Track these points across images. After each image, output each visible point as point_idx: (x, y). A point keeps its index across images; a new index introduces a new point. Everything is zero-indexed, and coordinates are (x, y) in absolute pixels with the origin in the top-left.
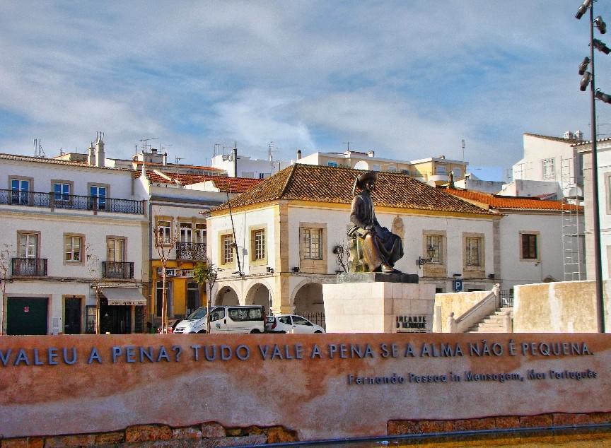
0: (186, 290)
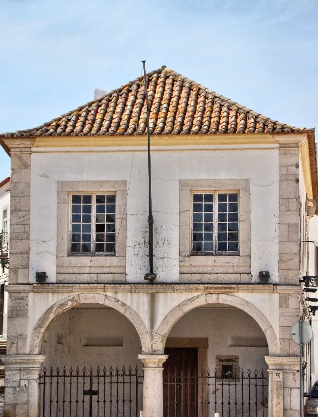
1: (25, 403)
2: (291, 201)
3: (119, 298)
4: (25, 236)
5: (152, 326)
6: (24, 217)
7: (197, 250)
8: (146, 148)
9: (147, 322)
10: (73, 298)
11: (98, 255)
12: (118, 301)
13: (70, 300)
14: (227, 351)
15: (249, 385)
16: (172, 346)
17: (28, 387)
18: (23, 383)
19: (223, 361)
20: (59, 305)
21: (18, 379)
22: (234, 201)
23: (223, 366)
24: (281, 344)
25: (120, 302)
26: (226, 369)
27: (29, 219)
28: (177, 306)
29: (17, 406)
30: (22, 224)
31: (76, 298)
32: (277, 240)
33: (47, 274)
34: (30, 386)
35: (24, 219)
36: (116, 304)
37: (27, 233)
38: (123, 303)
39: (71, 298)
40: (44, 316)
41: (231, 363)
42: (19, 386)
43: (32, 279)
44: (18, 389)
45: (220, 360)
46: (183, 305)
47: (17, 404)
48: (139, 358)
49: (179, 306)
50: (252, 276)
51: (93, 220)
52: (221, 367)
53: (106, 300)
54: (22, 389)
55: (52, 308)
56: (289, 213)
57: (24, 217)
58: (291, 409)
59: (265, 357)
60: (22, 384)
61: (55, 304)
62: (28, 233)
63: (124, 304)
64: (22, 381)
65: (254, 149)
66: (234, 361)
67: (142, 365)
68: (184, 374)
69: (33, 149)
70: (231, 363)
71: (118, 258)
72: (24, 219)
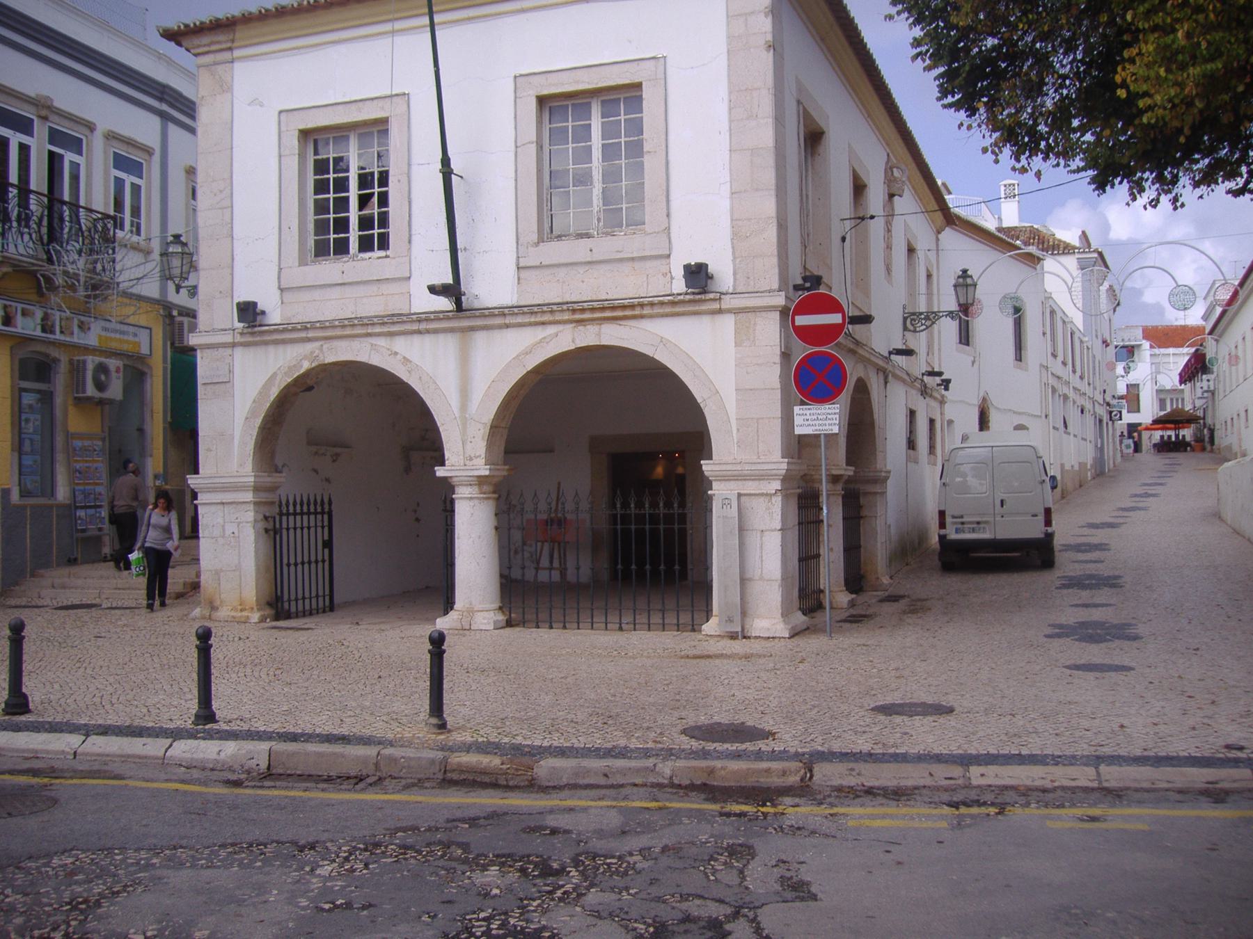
0: (12, 387)
3: (396, 349)
5: (464, 407)
7: (548, 232)
8: (426, 20)
9: (454, 402)
10: (312, 353)
11: (363, 259)
12: (396, 353)
13: (305, 358)
15: (509, 529)
18: (230, 528)
21: (222, 522)
24: (738, 430)
31: (317, 351)
32: (726, 190)
33: (260, 307)
38: (404, 358)
42: (223, 537)
43: (679, 285)
44: (221, 541)
46: (527, 353)
47: (221, 570)
48: (704, 468)
50: (672, 278)
51: (597, 154)
53: (373, 352)
55: (275, 375)
57: (221, 191)
58: (761, 578)
60: (228, 532)
61: (279, 369)
65: (294, 49)
67: (446, 489)
68: (664, 504)
69: (237, 53)
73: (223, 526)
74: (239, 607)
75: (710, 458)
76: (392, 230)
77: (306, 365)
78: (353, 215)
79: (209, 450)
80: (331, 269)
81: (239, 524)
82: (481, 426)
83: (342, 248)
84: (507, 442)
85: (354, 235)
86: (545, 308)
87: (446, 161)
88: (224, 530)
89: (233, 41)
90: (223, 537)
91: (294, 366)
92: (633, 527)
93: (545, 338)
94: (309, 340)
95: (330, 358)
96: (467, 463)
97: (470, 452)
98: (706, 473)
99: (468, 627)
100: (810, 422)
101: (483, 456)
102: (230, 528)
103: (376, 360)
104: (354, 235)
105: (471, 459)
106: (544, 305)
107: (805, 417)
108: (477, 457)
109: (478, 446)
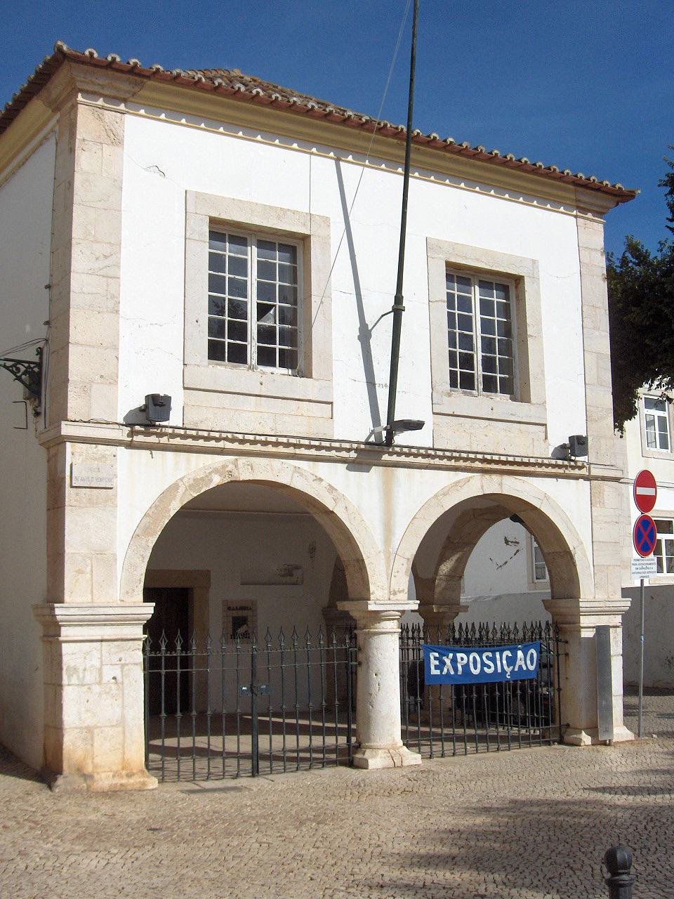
1: (115, 723)
2: (598, 310)
4: (111, 304)
5: (387, 540)
6: (106, 257)
10: (224, 467)
12: (321, 480)
13: (216, 471)
14: (239, 595)
16: (158, 585)
17: (122, 683)
18: (108, 673)
19: (233, 609)
20: (191, 481)
21: (98, 664)
22: (500, 302)
23: (234, 618)
25: (323, 483)
26: (238, 622)
27: (118, 266)
28: (433, 498)
29: (96, 731)
30: (102, 272)
34: (126, 681)
35: (107, 262)
36: (315, 484)
37: (113, 297)
38: (330, 485)
39: (219, 465)
40: (156, 507)
41: (244, 613)
42: (100, 683)
44: (96, 689)
45: (229, 609)
46: (444, 495)
49: (436, 496)
52: (231, 619)
53: (296, 475)
54: (108, 690)
55: (174, 488)
56: (597, 333)
57: (106, 257)
59: (337, 603)
60: (107, 677)
61: (181, 479)
62: (115, 298)
63: (331, 489)
64: (106, 669)
66: (250, 609)
68: (166, 647)
70: (244, 613)
71: (317, 383)
72: (107, 262)
73: (100, 670)
74: (124, 772)
75: (62, 601)
76: (205, 338)
77: (217, 480)
78: (253, 324)
79: (80, 572)
80: (225, 373)
81: (123, 666)
82: (405, 561)
83: (238, 356)
84: (150, 574)
85: (252, 346)
86: (455, 454)
87: (399, 299)
88: (101, 675)
89: (134, 94)
90: (100, 683)
91: (202, 478)
92: (163, 671)
93: (459, 482)
94: (222, 452)
95: (245, 475)
96: (392, 597)
97: (395, 587)
98: (59, 618)
99: (400, 765)
100: (638, 571)
101: (406, 590)
102: (108, 673)
103: (298, 484)
104: (252, 346)
105: (395, 594)
106: (455, 451)
107: (636, 567)
108: (400, 592)
109: (403, 580)
